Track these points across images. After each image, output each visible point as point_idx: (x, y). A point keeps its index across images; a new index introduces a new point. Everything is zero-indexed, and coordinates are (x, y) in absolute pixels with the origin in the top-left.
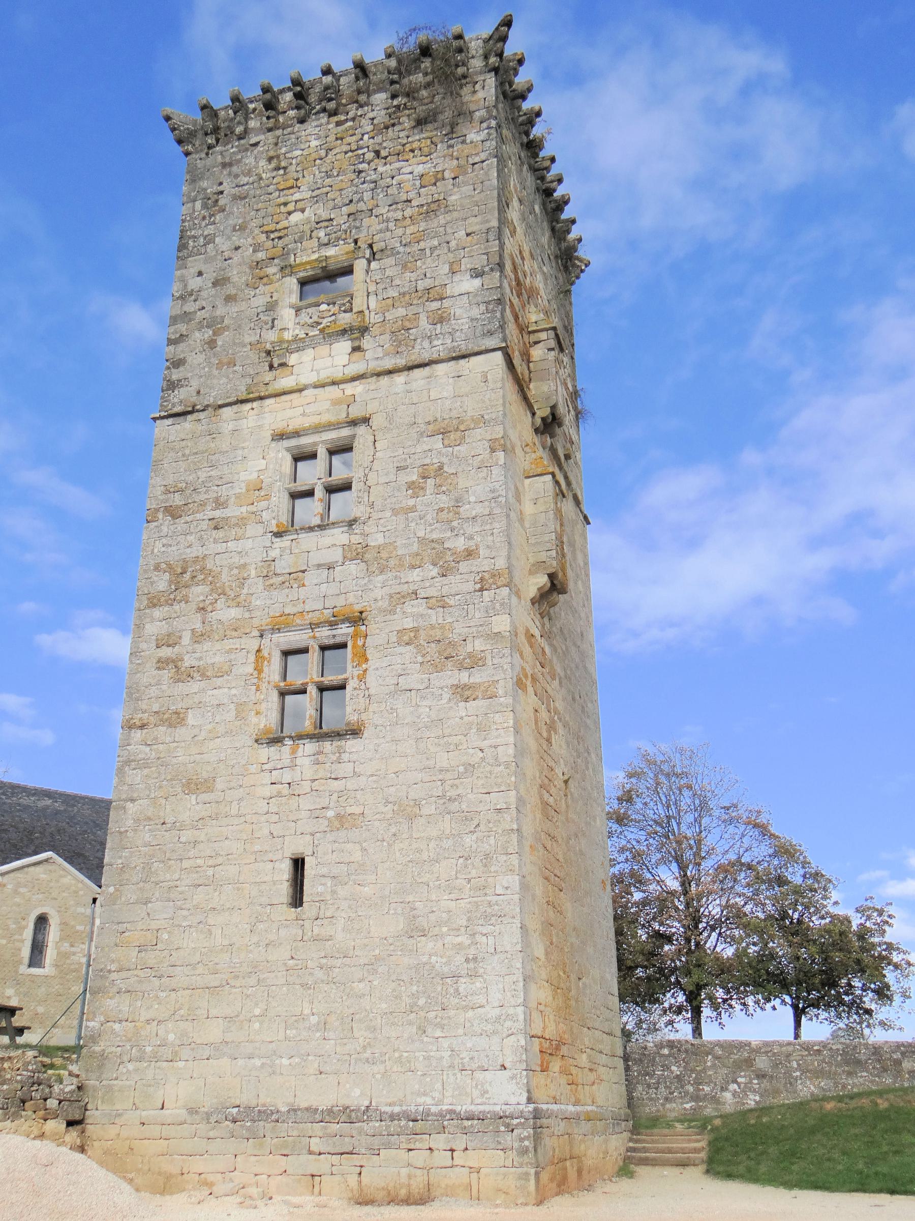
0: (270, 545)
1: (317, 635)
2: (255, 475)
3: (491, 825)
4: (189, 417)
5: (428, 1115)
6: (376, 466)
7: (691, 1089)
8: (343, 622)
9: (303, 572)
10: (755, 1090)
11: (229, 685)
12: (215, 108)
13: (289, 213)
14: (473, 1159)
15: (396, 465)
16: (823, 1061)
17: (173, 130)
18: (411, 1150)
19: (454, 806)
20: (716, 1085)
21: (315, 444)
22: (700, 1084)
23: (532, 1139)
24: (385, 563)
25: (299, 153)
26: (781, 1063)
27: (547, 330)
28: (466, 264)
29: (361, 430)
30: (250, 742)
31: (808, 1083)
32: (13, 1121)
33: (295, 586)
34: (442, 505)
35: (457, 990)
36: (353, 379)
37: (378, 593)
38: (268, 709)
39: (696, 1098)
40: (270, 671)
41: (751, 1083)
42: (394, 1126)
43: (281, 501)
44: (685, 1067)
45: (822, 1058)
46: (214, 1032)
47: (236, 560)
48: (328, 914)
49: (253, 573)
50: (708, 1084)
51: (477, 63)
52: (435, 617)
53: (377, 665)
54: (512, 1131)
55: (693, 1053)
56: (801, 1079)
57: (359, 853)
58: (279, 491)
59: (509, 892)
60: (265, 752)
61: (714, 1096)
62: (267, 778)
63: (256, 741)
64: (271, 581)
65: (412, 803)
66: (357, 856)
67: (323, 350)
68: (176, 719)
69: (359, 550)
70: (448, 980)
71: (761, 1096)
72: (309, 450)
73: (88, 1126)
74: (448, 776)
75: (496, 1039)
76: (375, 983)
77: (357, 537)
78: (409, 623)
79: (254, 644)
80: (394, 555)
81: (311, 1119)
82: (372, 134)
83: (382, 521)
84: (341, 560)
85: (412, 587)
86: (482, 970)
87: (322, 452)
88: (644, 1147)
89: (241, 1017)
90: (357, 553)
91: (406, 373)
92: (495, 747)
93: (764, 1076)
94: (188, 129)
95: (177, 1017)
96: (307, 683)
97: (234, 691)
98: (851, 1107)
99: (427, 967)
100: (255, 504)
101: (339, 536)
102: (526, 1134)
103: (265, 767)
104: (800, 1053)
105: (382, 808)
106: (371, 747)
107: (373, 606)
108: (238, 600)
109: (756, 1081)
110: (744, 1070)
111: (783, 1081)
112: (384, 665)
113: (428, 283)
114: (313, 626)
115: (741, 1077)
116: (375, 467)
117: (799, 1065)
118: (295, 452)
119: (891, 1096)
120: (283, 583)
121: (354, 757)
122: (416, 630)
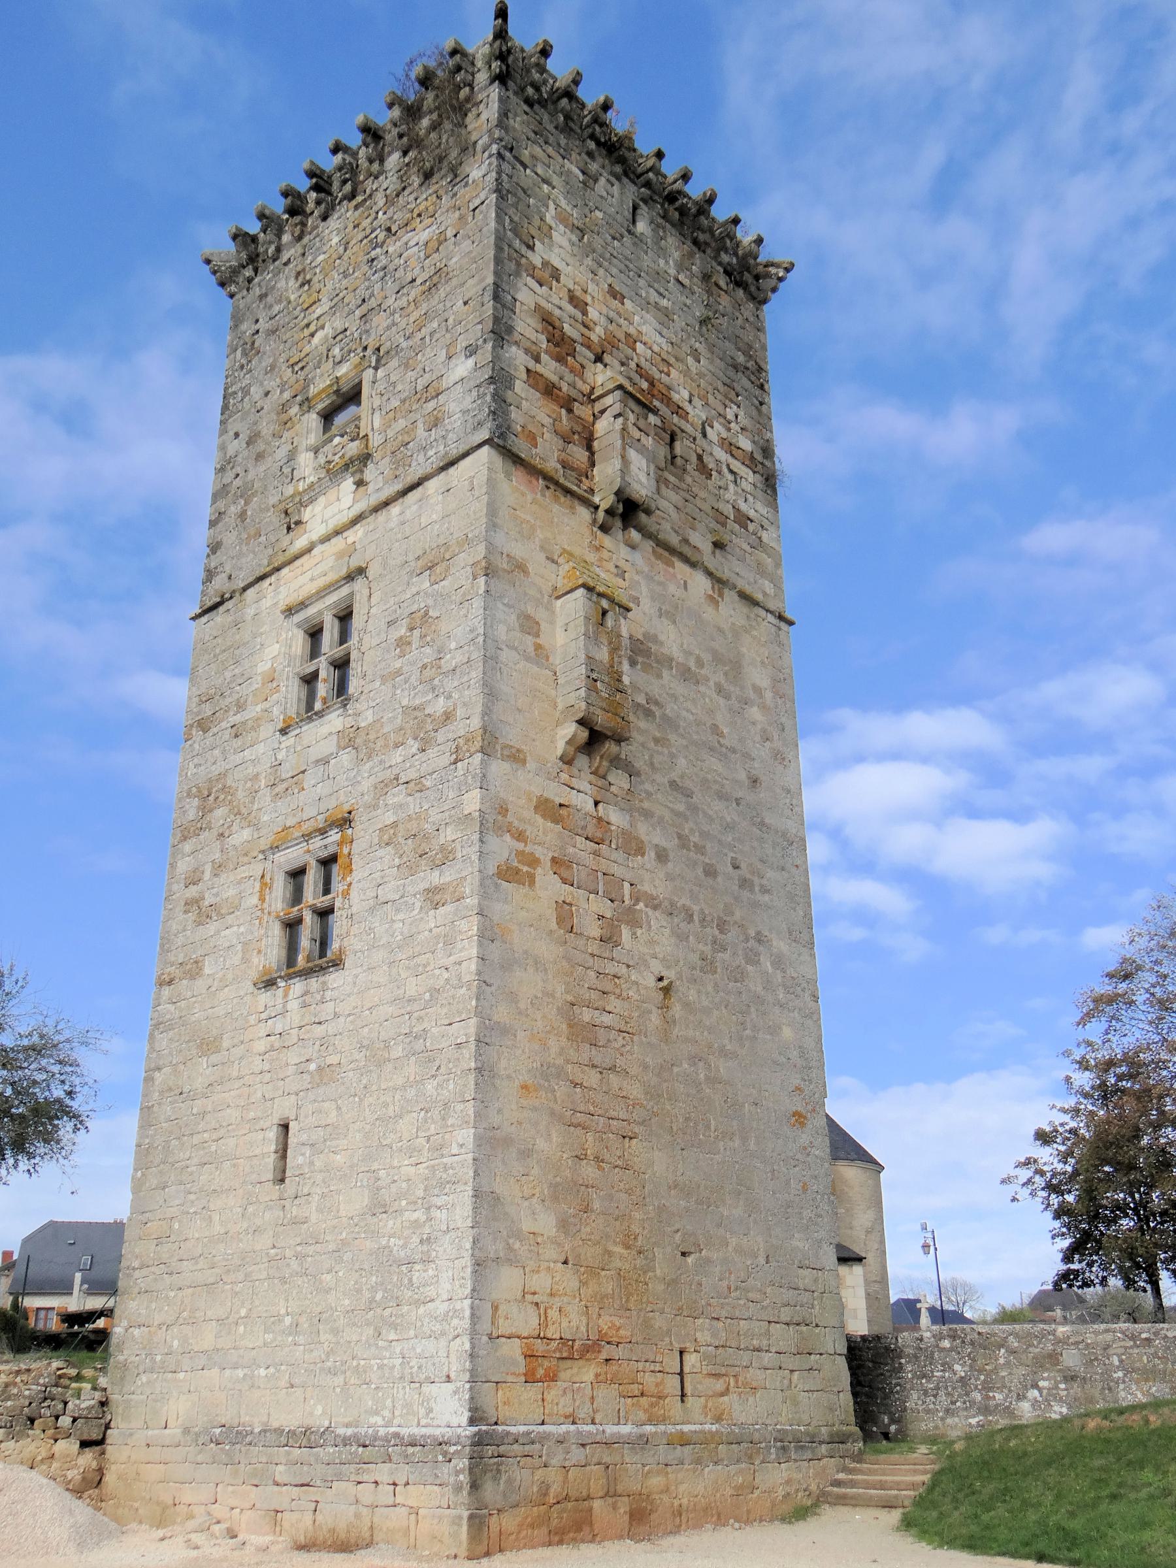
3: (451, 1065)
4: (221, 609)
5: (375, 1439)
7: (977, 1396)
9: (303, 772)
10: (1061, 1398)
12: (251, 233)
13: (312, 335)
14: (411, 1496)
16: (1155, 1355)
17: (214, 273)
18: (359, 1483)
19: (419, 1045)
20: (1010, 1391)
21: (320, 613)
22: (991, 1389)
23: (467, 1472)
25: (321, 258)
26: (1096, 1359)
27: (611, 391)
28: (462, 343)
29: (359, 585)
31: (1134, 1387)
32: (17, 1441)
33: (296, 791)
34: (426, 660)
35: (410, 1280)
36: (355, 521)
39: (985, 1410)
41: (1057, 1388)
42: (345, 1452)
44: (971, 1366)
45: (1152, 1350)
46: (207, 1338)
48: (306, 1191)
50: (1000, 1389)
51: (482, 77)
52: (413, 805)
54: (450, 1461)
55: (980, 1346)
56: (1124, 1382)
57: (334, 1113)
58: (287, 679)
59: (463, 1151)
60: (265, 997)
61: (1008, 1408)
62: (263, 1030)
64: (277, 790)
65: (382, 1045)
66: (333, 1117)
67: (332, 494)
68: (194, 970)
70: (404, 1268)
71: (1070, 1408)
73: (109, 1447)
74: (416, 1006)
75: (443, 1342)
76: (341, 1274)
78: (389, 818)
81: (277, 1443)
82: (384, 209)
85: (395, 771)
86: (434, 1254)
88: (852, 1480)
89: (231, 1320)
91: (401, 500)
92: (460, 963)
93: (1073, 1378)
94: (231, 267)
95: (181, 1321)
97: (242, 929)
98: (1118, 1424)
99: (386, 1250)
102: (461, 1465)
103: (263, 1016)
104: (1122, 1344)
105: (357, 1056)
106: (350, 979)
109: (1062, 1386)
110: (1047, 1370)
111: (1100, 1385)
113: (427, 378)
114: (307, 837)
115: (1043, 1379)
117: (1121, 1361)
119: (1166, 1410)
121: (335, 994)
122: (395, 825)
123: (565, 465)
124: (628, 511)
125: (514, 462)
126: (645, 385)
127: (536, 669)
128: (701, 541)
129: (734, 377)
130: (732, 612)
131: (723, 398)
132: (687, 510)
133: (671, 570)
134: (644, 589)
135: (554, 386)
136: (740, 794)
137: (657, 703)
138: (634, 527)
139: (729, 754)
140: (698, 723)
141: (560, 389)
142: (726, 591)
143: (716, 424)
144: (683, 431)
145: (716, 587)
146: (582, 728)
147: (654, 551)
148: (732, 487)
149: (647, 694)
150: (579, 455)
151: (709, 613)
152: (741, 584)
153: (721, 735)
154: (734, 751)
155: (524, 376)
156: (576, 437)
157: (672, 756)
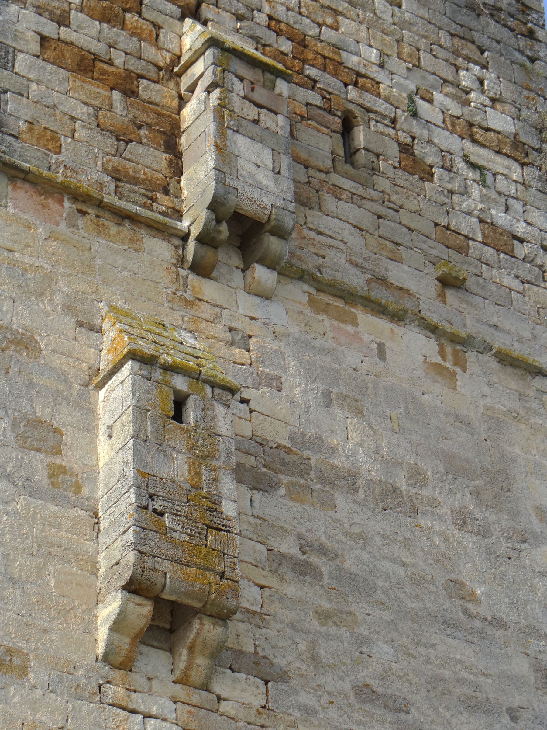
123: (118, 176)
124: (239, 233)
125: (12, 179)
126: (287, 46)
127: (52, 508)
128: (414, 278)
129: (473, 24)
130: (486, 390)
131: (450, 56)
132: (381, 232)
133: (349, 328)
134: (292, 364)
135: (96, 58)
136: (517, 701)
137: (323, 551)
138: (261, 262)
139: (489, 630)
140: (417, 581)
141: (110, 63)
142: (471, 356)
143: (437, 96)
144: (368, 110)
145: (449, 349)
146: (137, 599)
147: (311, 301)
148: (475, 191)
149: (300, 537)
150: (150, 160)
151: (435, 394)
152: (500, 342)
153: (473, 598)
154: (502, 625)
155: (35, 47)
156: (144, 132)
157: (361, 641)
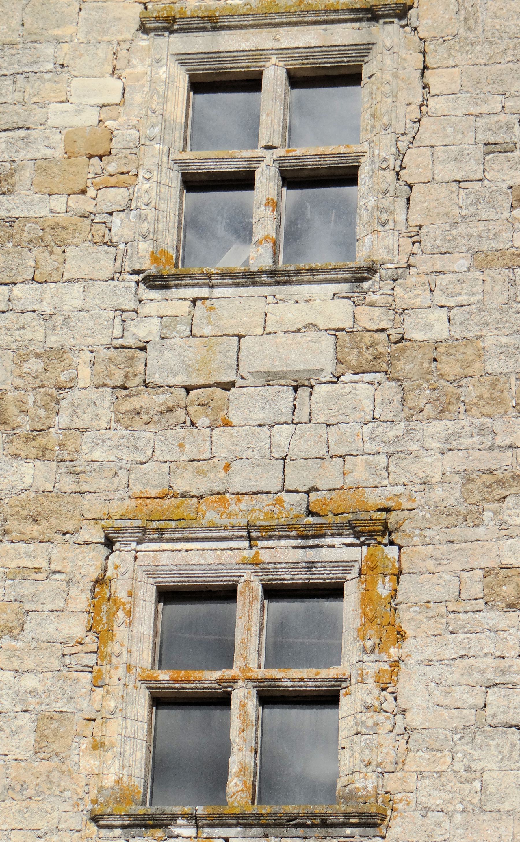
0: (132, 305)
1: (265, 556)
2: (90, 117)
6: (428, 131)
8: (338, 530)
9: (227, 386)
11: (16, 664)
15: (482, 137)
21: (261, 54)
24: (450, 388)
30: (78, 820)
37: (433, 466)
38: (126, 738)
40: (131, 637)
43: (160, 191)
47: (37, 334)
49: (85, 376)
53: (429, 653)
58: (159, 165)
63: (95, 819)
64: (136, 403)
69: (381, 348)
72: (241, 66)
77: (377, 312)
79: (89, 562)
80: (476, 368)
83: (442, 280)
84: (330, 367)
87: (274, 76)
90: (374, 356)
96: (235, 680)
97: (29, 682)
100: (91, 192)
101: (323, 304)
107: (419, 499)
108: (42, 441)
112: (449, 654)
114: (253, 534)
116: (426, 136)
118: (202, 68)
120: (170, 410)
